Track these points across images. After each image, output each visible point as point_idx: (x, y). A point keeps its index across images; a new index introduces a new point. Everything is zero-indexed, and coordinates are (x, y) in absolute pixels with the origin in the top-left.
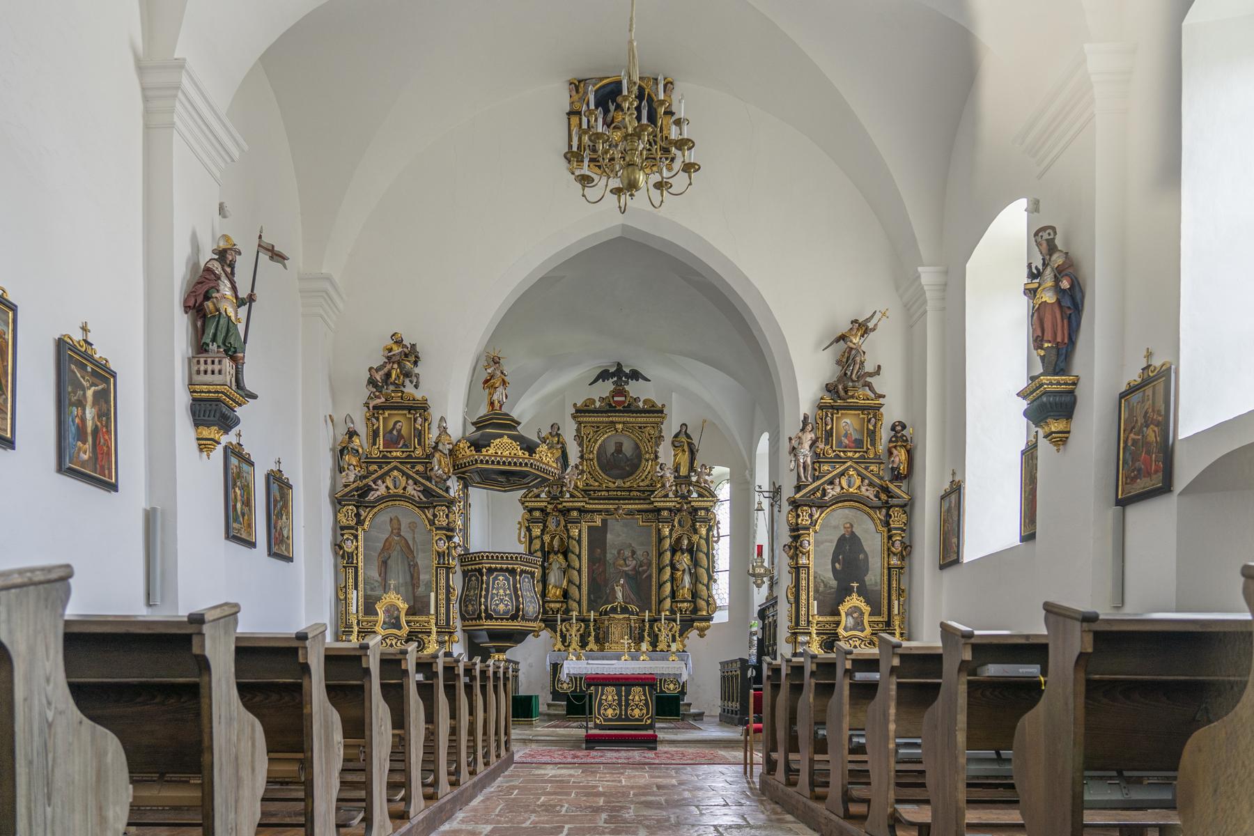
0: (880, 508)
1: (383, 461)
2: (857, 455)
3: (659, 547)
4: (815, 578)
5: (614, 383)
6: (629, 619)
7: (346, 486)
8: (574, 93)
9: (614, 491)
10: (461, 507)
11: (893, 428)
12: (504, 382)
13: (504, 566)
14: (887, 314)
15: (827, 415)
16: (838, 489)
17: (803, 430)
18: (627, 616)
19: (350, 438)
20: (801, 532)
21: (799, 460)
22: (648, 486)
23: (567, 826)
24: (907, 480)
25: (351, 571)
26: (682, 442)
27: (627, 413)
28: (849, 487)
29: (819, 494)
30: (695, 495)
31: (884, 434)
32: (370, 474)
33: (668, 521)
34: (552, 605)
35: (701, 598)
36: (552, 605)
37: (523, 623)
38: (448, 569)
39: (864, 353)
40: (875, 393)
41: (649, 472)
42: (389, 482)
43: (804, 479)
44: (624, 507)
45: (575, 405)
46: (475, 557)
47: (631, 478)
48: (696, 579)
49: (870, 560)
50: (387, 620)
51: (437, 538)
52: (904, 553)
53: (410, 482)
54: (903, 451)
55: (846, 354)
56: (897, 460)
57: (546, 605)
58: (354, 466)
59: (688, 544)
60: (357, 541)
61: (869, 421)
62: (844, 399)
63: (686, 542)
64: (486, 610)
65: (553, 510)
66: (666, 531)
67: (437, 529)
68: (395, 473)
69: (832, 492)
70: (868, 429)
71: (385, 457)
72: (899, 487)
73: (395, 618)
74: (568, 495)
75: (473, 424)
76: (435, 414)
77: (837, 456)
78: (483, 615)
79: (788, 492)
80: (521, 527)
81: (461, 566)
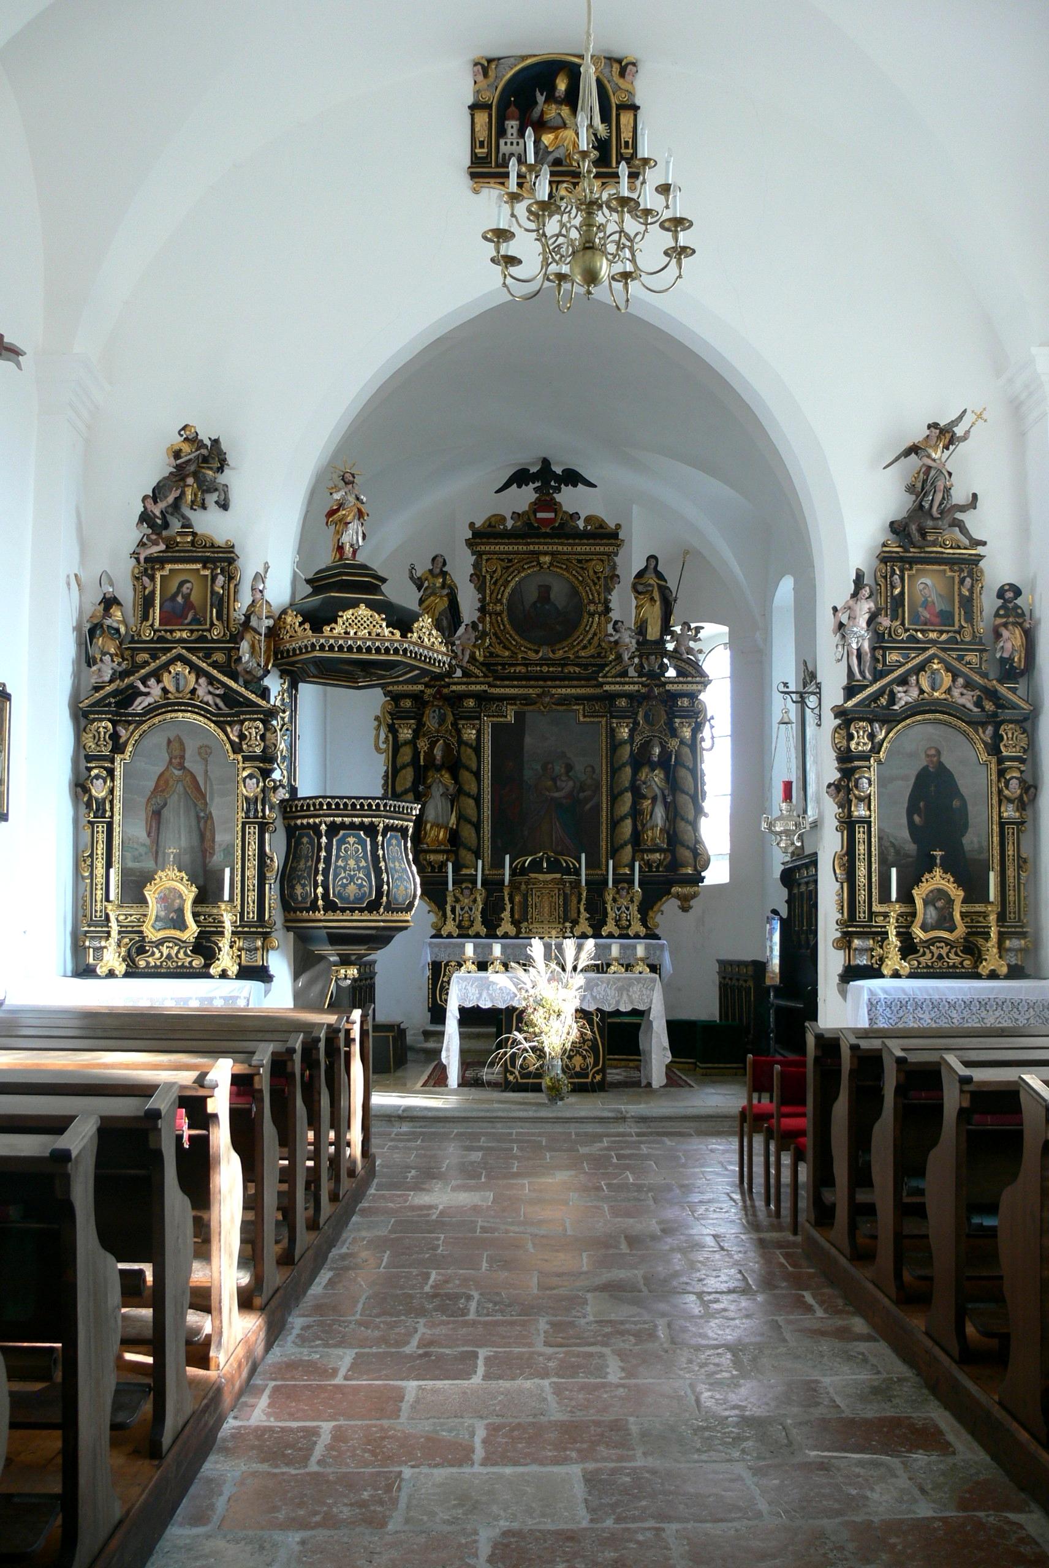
0: (984, 725)
1: (160, 646)
2: (944, 637)
3: (612, 758)
4: (880, 839)
5: (536, 490)
6: (562, 881)
7: (97, 689)
8: (480, 78)
9: (537, 665)
10: (286, 720)
11: (1001, 594)
12: (360, 514)
13: (357, 820)
14: (984, 416)
15: (893, 573)
16: (915, 693)
17: (855, 595)
18: (558, 876)
19: (107, 609)
20: (857, 763)
21: (849, 644)
22: (592, 656)
23: (483, 1353)
24: (1025, 678)
25: (101, 828)
26: (650, 585)
27: (559, 538)
28: (933, 689)
29: (883, 701)
30: (671, 673)
31: (988, 603)
32: (135, 668)
33: (622, 715)
34: (432, 857)
35: (683, 846)
36: (432, 857)
37: (389, 916)
38: (263, 828)
39: (950, 474)
40: (970, 538)
41: (595, 634)
42: (168, 681)
43: (858, 676)
44: (554, 691)
45: (472, 525)
46: (308, 805)
47: (565, 643)
48: (674, 814)
49: (970, 808)
50: (162, 914)
51: (245, 774)
52: (1025, 799)
53: (202, 680)
54: (1017, 632)
55: (921, 475)
56: (1009, 645)
57: (421, 857)
58: (111, 655)
59: (660, 753)
60: (113, 780)
61: (962, 582)
62: (919, 547)
63: (657, 751)
64: (326, 895)
65: (434, 697)
66: (624, 733)
67: (246, 759)
68: (179, 667)
69: (905, 697)
70: (960, 594)
71: (161, 639)
72: (1013, 690)
73: (175, 911)
74: (459, 673)
75: (308, 581)
76: (248, 567)
77: (912, 639)
78: (320, 902)
79: (833, 694)
80: (379, 726)
81: (284, 818)
